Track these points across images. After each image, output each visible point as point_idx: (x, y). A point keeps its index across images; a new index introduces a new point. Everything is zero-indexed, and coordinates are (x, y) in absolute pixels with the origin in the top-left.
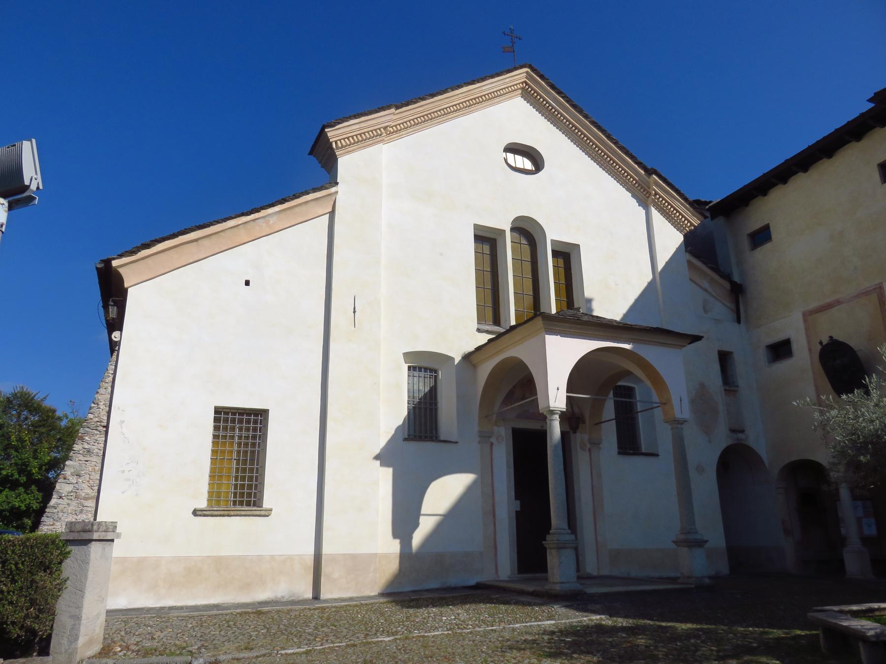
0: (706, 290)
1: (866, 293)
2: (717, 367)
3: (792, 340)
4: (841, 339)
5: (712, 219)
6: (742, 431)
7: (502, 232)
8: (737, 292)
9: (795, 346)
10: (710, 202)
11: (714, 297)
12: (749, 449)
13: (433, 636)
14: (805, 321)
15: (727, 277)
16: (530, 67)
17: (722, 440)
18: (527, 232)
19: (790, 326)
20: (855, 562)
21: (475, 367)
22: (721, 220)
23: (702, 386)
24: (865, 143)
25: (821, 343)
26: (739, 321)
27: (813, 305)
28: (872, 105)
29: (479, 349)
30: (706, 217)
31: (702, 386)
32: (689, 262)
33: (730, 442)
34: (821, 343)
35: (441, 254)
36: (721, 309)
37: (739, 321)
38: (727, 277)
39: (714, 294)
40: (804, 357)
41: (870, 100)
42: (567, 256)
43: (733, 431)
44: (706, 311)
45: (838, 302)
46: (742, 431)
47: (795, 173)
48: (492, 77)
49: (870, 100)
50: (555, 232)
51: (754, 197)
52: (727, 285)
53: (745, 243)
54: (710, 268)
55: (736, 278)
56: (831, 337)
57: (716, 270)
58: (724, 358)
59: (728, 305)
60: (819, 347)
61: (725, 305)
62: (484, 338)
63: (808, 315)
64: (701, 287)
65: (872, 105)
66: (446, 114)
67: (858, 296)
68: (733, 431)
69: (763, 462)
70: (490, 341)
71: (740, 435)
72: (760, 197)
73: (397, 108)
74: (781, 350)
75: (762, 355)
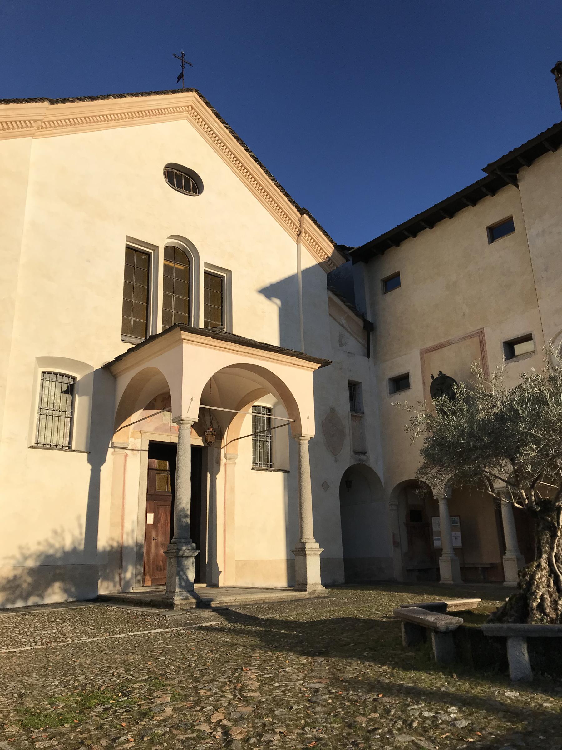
0: (342, 326)
1: (471, 336)
2: (346, 395)
3: (410, 374)
4: (448, 375)
5: (353, 264)
6: (365, 453)
7: (156, 248)
8: (369, 328)
9: (412, 380)
10: (353, 248)
11: (349, 332)
12: (370, 470)
13: (21, 652)
14: (422, 358)
15: (362, 316)
16: (197, 91)
17: (347, 460)
18: (181, 255)
19: (409, 362)
20: (446, 570)
21: (115, 378)
22: (361, 264)
23: (333, 410)
24: (478, 208)
25: (432, 377)
26: (368, 356)
27: (430, 344)
28: (485, 175)
29: (118, 359)
30: (347, 260)
31: (333, 410)
32: (330, 299)
33: (353, 463)
34: (432, 377)
35: (89, 261)
36: (354, 344)
37: (368, 356)
38: (362, 316)
39: (349, 329)
40: (419, 387)
41: (484, 170)
42: (218, 284)
43: (356, 453)
44: (341, 345)
45: (449, 343)
46: (365, 453)
47: (423, 228)
48: (157, 93)
49: (484, 170)
50: (208, 256)
51: (389, 247)
52: (361, 324)
53: (379, 286)
54: (348, 306)
55: (369, 318)
56: (440, 372)
57: (353, 308)
58: (354, 388)
59: (361, 341)
60: (431, 380)
61: (359, 341)
62: (124, 348)
63: (424, 353)
64: (339, 323)
65: (485, 175)
66: (107, 120)
67: (464, 338)
68: (356, 453)
69: (381, 482)
70: (130, 350)
71: (363, 457)
72: (394, 248)
73: (52, 102)
74: (401, 383)
75: (385, 386)
